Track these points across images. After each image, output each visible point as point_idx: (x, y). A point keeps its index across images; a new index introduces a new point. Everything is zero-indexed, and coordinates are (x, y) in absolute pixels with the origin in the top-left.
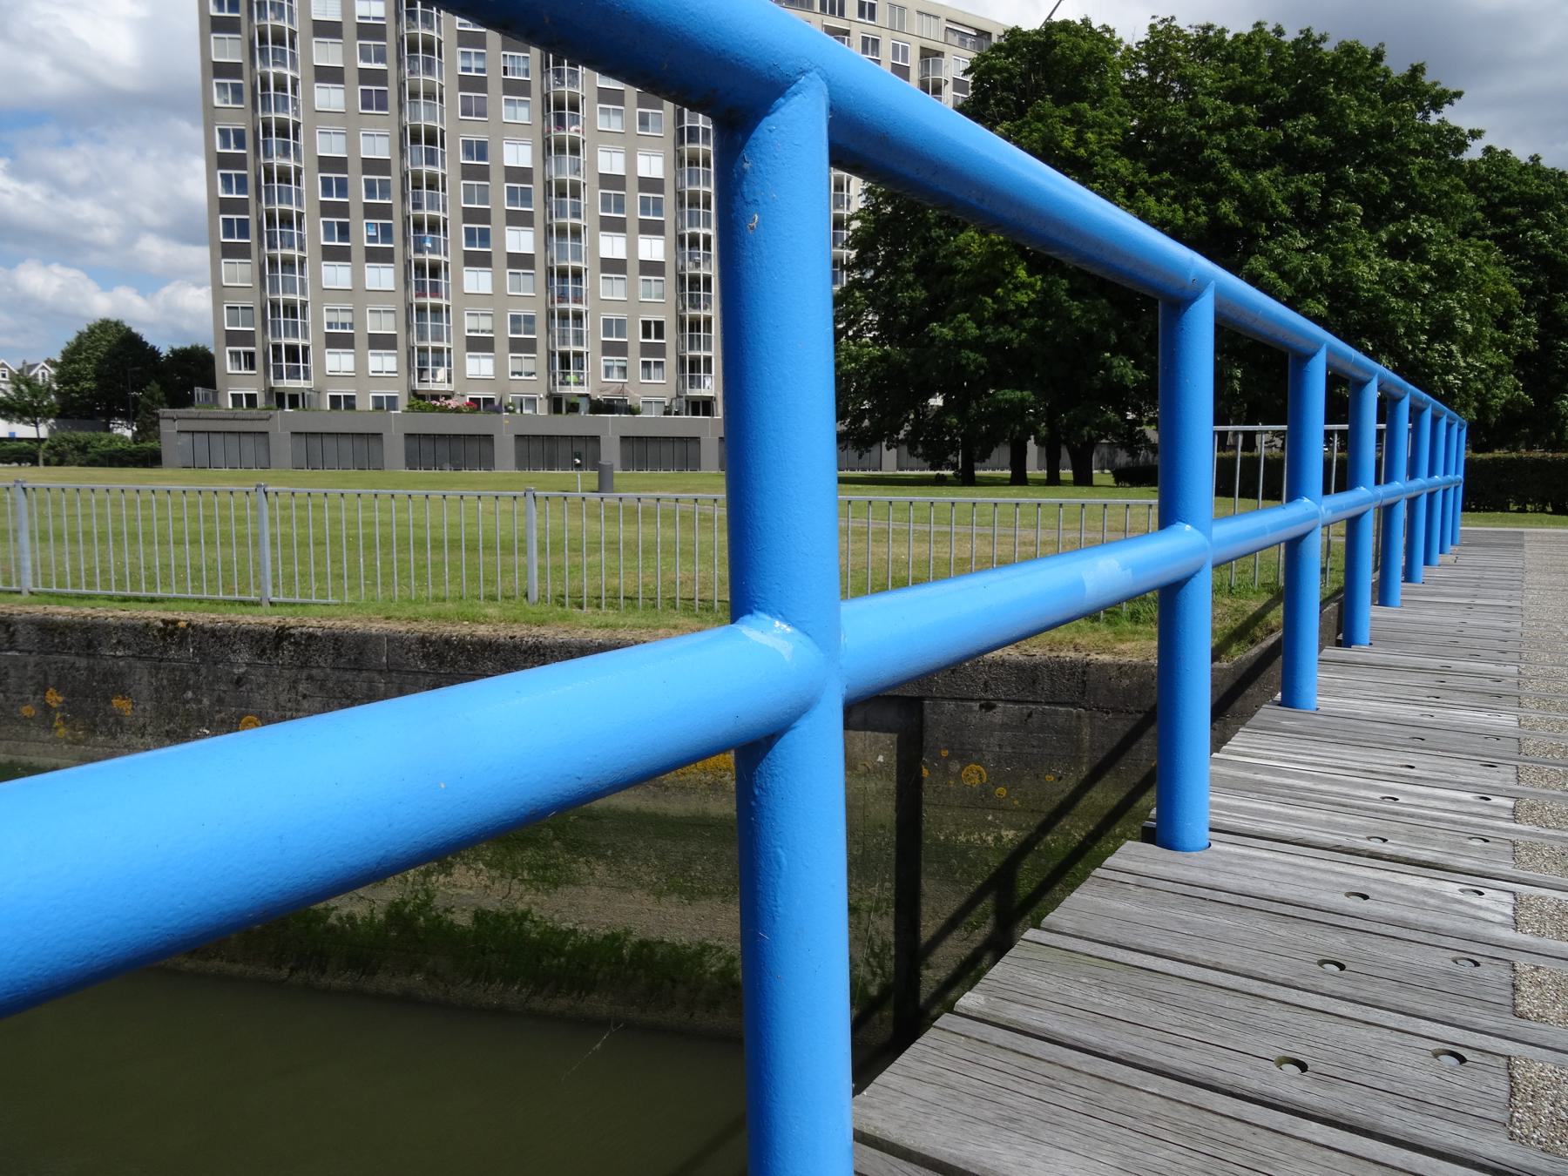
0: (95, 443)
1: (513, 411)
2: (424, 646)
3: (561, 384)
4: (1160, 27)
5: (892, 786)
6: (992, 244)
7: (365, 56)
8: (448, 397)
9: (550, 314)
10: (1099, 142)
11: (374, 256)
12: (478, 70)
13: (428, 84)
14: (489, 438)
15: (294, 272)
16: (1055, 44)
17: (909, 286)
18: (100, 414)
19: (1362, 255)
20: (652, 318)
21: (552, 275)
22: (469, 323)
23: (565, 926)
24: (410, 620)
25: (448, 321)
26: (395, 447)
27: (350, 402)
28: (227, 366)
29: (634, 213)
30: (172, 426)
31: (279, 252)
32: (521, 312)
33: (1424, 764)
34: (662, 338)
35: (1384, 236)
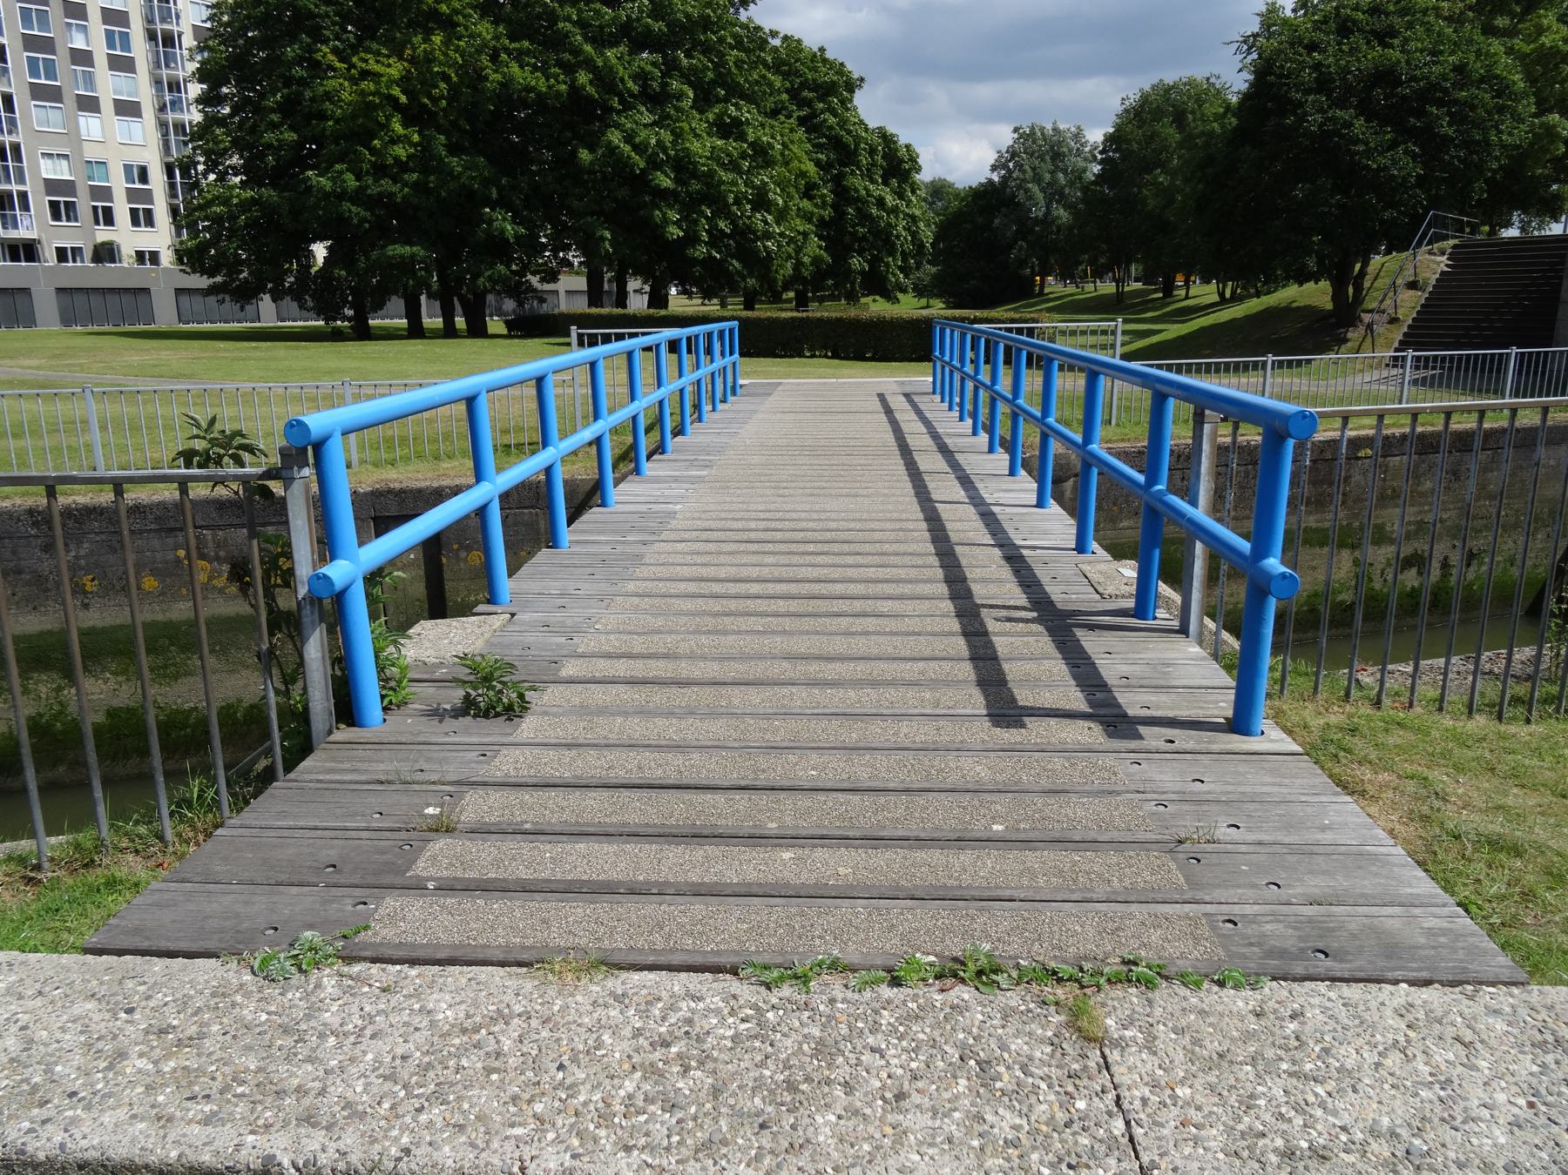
2: (32, 516)
5: (422, 573)
6: (363, 93)
17: (274, 126)
23: (186, 706)
33: (674, 485)
35: (711, 117)
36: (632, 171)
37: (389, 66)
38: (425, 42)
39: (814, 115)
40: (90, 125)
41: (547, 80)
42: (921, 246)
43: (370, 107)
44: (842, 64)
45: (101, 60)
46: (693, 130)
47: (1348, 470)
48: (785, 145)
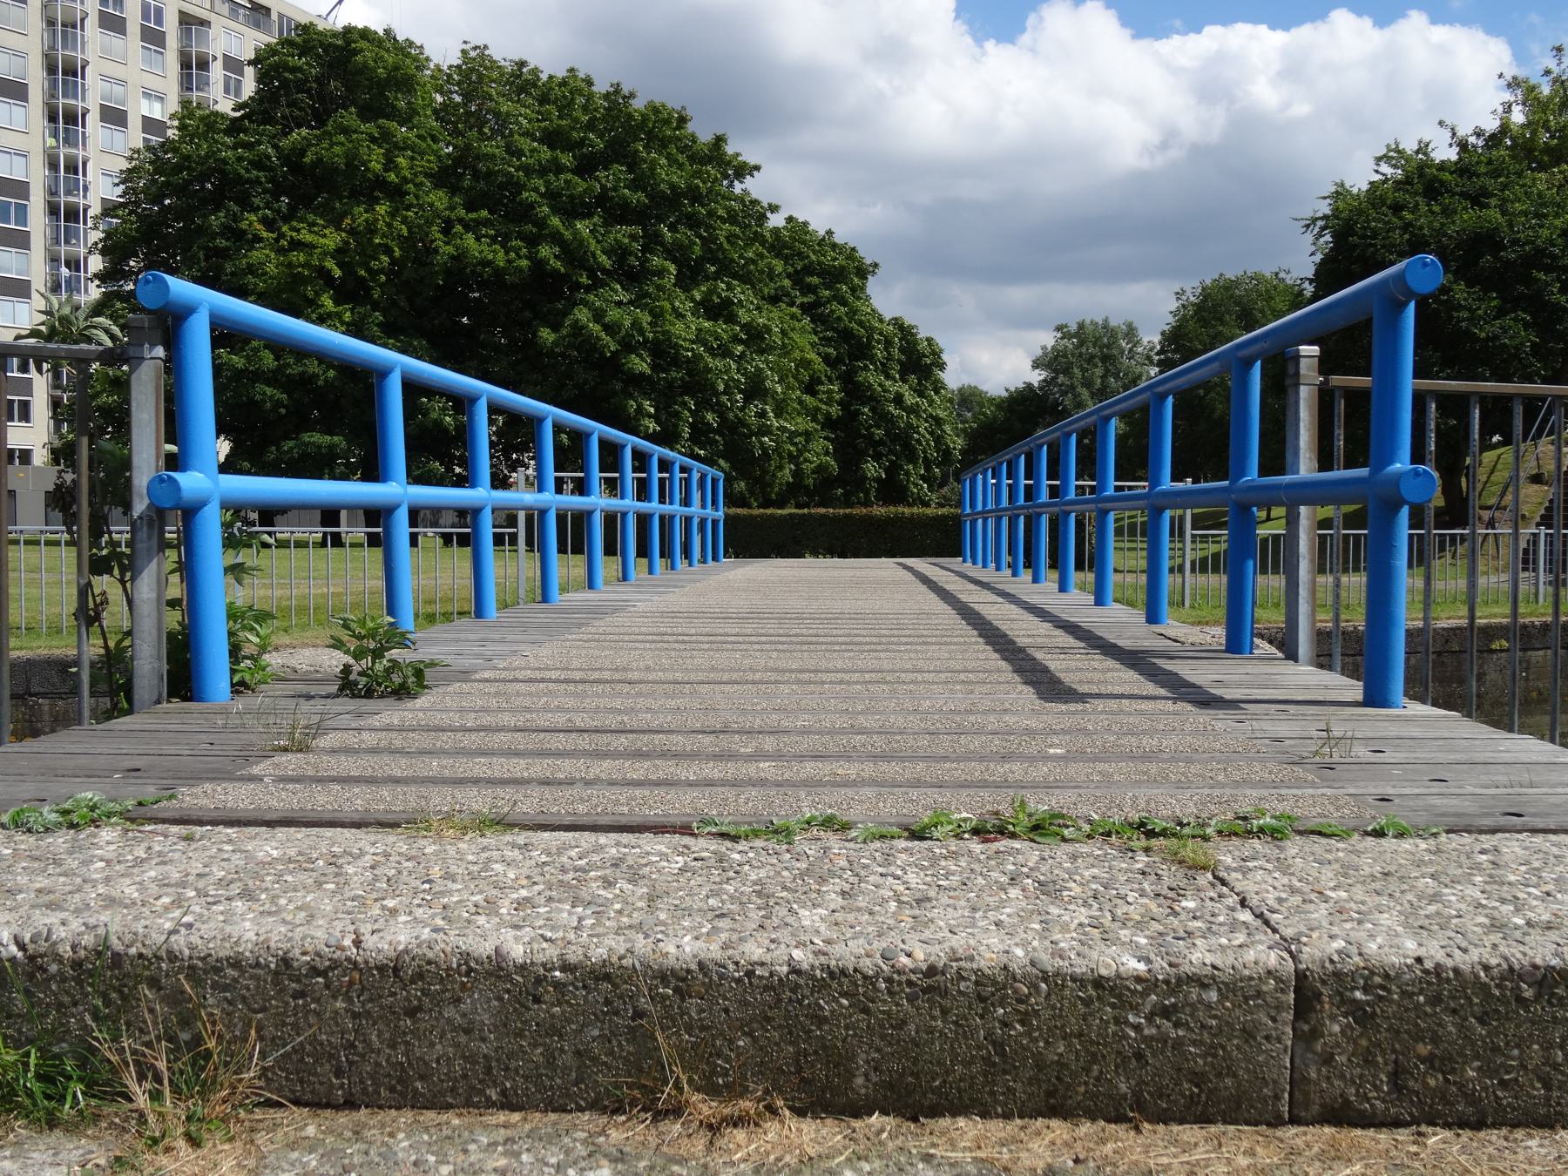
4: (473, 54)
6: (290, 265)
16: (356, 52)
36: (602, 354)
37: (324, 236)
38: (366, 211)
39: (817, 304)
41: (507, 253)
42: (947, 453)
44: (853, 249)
46: (675, 309)
47: (1481, 666)
48: (783, 332)
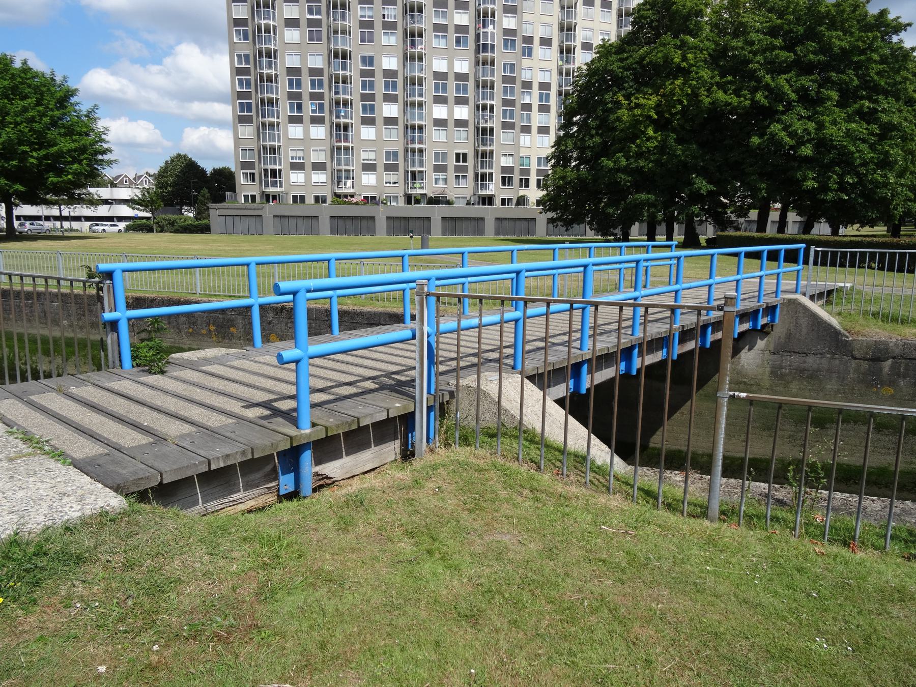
0: (178, 221)
1: (386, 204)
3: (411, 188)
6: (634, 116)
7: (310, 11)
8: (352, 196)
9: (406, 150)
10: (695, 58)
11: (316, 120)
12: (369, 17)
13: (344, 26)
14: (373, 218)
15: (274, 130)
18: (177, 204)
19: (834, 123)
20: (461, 151)
21: (407, 128)
22: (364, 156)
24: (322, 304)
25: (353, 155)
26: (325, 223)
27: (303, 198)
28: (241, 180)
29: (452, 93)
30: (215, 212)
31: (267, 120)
32: (391, 149)
34: (466, 162)
40: (525, 139)
43: (638, 122)
45: (535, 108)
